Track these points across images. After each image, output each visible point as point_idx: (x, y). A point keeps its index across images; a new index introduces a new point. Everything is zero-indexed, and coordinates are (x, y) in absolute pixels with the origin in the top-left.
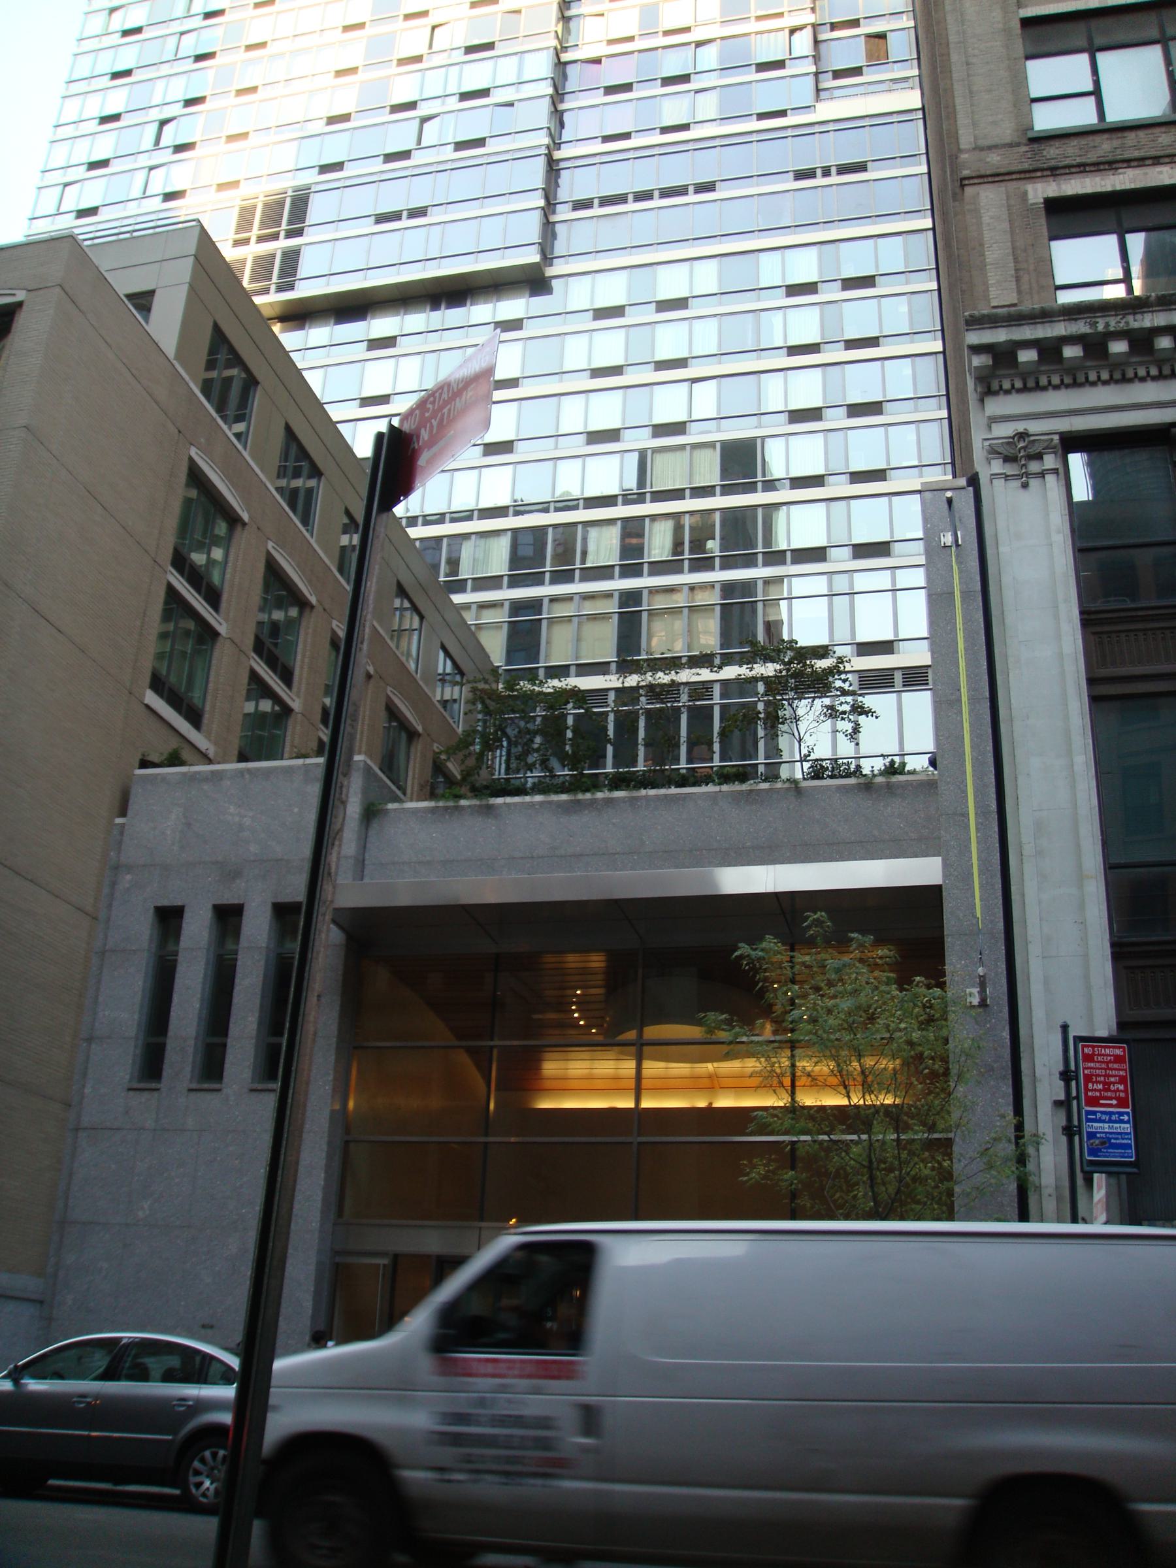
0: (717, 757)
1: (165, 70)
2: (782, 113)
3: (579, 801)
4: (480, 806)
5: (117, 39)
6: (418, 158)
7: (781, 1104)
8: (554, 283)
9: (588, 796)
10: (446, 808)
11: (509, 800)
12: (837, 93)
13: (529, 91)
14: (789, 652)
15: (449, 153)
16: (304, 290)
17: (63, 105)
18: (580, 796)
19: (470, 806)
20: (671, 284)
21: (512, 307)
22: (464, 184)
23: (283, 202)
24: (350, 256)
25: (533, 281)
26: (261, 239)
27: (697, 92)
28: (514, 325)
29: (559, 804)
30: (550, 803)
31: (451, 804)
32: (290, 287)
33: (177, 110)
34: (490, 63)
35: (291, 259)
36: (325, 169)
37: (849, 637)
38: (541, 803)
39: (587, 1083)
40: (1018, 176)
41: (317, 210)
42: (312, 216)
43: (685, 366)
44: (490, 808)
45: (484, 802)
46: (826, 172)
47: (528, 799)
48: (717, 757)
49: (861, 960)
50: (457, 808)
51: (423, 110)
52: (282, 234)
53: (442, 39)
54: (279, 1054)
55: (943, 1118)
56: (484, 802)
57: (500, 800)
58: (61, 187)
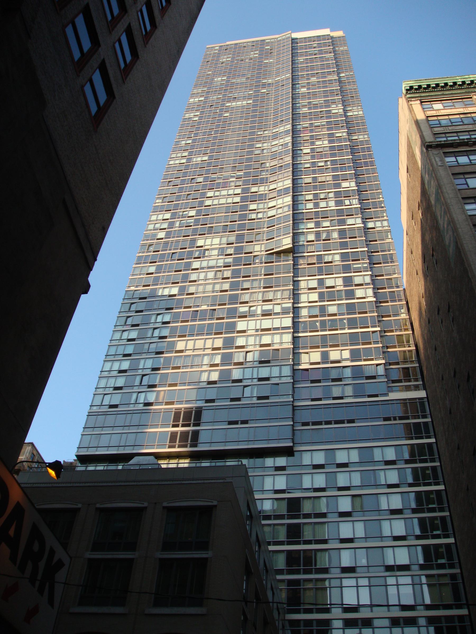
1: (144, 356)
2: (376, 396)
5: (125, 342)
6: (243, 402)
8: (295, 453)
12: (394, 388)
13: (284, 380)
14: (212, 242)
15: (255, 401)
16: (201, 448)
17: (104, 363)
20: (341, 457)
21: (281, 461)
22: (261, 413)
23: (192, 412)
24: (218, 437)
25: (288, 452)
26: (183, 426)
27: (345, 385)
28: (282, 468)
32: (196, 446)
33: (148, 371)
34: (269, 368)
35: (196, 434)
36: (207, 401)
37: (422, 602)
41: (205, 416)
42: (204, 419)
43: (349, 490)
46: (395, 419)
51: (245, 383)
52: (192, 425)
53: (250, 357)
55: (366, 164)
58: (102, 395)
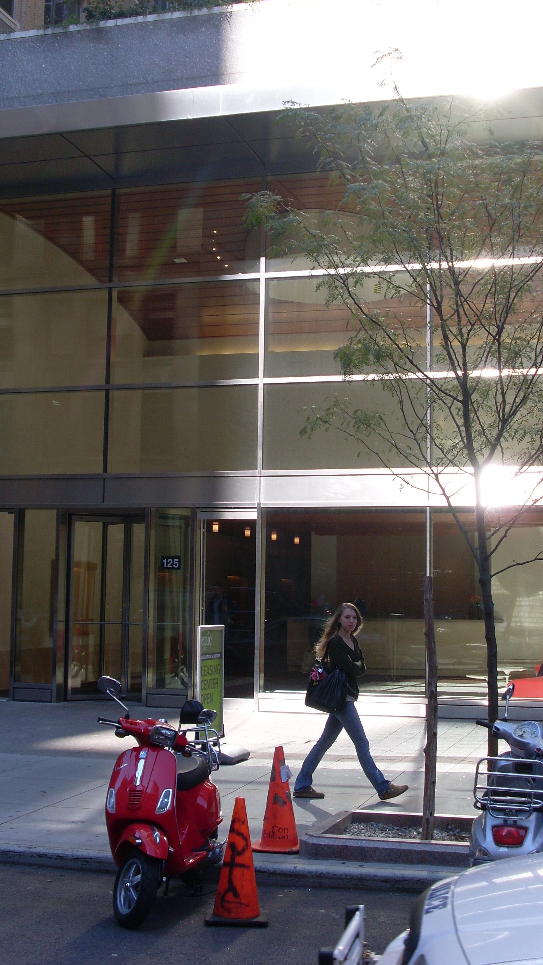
0: (261, 387)
3: (195, 18)
4: (90, 30)
7: (158, 891)
9: (205, 11)
10: (55, 35)
11: (120, 22)
18: (196, 13)
19: (79, 32)
29: (173, 23)
30: (162, 21)
31: (60, 30)
38: (154, 23)
39: (456, 660)
40: (188, 594)
44: (100, 31)
45: (94, 26)
47: (140, 19)
48: (261, 387)
49: (404, 104)
50: (65, 34)
54: (268, 651)
56: (94, 26)
57: (111, 23)
